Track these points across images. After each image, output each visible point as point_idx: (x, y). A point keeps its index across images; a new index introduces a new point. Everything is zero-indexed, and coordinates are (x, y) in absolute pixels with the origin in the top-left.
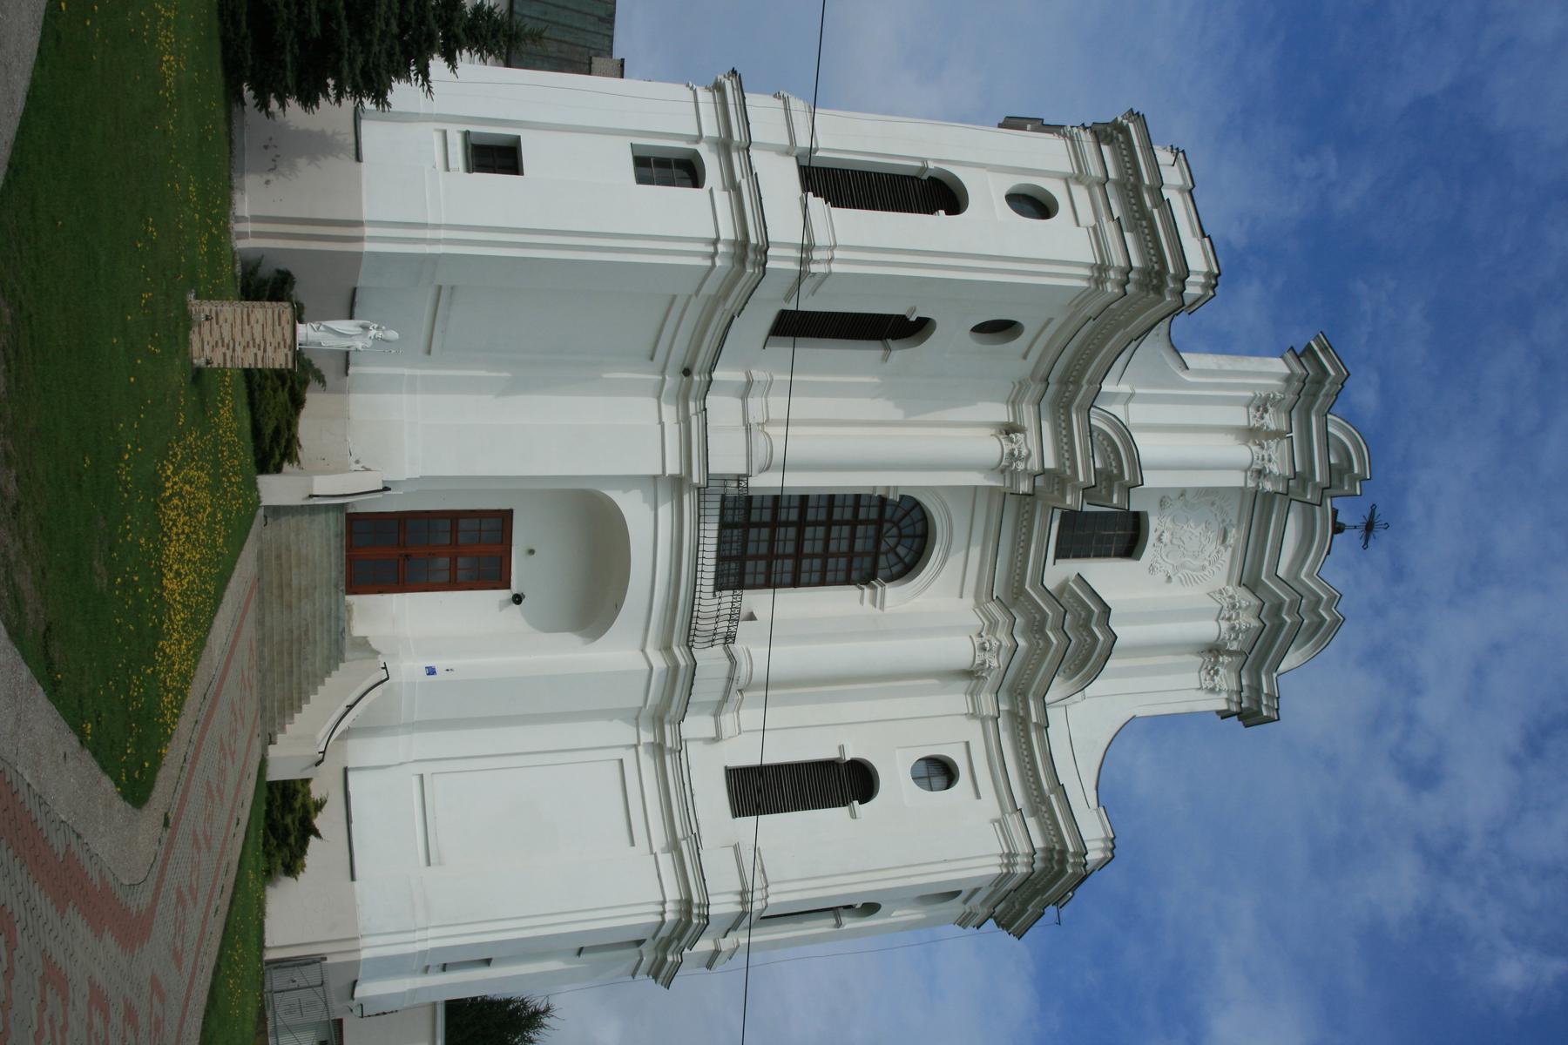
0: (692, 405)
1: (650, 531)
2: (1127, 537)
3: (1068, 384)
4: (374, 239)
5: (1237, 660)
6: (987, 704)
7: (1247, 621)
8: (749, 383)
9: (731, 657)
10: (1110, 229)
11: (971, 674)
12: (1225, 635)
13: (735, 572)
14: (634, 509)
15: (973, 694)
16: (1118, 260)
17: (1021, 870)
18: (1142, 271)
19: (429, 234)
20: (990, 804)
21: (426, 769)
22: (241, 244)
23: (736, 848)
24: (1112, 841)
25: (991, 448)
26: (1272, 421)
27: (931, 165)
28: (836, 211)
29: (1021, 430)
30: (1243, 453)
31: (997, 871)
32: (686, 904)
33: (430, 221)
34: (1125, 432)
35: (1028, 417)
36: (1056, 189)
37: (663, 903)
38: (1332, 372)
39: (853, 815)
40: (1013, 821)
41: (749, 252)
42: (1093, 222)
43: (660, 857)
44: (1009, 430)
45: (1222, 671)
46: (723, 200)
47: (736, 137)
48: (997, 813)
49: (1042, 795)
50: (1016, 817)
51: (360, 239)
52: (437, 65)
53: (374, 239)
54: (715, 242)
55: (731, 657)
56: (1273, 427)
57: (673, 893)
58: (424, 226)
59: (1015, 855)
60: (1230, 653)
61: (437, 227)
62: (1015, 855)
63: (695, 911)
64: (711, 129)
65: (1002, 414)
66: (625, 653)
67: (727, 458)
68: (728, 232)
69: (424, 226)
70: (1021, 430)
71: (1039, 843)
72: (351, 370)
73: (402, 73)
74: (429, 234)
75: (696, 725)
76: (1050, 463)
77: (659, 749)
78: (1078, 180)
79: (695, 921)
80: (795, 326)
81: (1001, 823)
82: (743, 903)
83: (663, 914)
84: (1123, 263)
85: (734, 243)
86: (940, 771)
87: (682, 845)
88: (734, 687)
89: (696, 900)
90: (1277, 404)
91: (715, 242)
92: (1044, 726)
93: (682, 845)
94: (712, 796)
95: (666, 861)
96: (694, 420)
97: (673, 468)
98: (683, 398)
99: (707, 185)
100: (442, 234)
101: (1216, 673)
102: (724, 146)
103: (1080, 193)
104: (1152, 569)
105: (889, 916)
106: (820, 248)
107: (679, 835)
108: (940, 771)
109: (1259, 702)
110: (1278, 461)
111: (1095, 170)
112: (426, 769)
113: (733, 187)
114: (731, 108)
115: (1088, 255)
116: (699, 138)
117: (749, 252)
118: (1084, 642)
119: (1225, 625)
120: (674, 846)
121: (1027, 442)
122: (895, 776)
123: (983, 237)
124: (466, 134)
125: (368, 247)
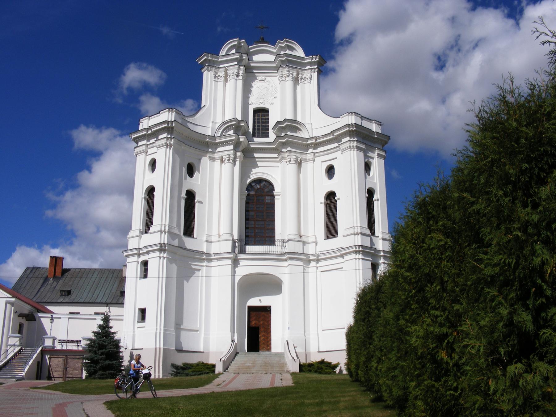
0: (212, 257)
1: (246, 268)
2: (262, 113)
3: (206, 145)
4: (160, 345)
5: (301, 72)
6: (309, 157)
7: (285, 71)
8: (207, 241)
9: (288, 241)
10: (158, 143)
11: (299, 163)
12: (290, 78)
13: (270, 239)
14: (243, 270)
15: (306, 161)
16: (164, 141)
17: (355, 144)
18: (168, 134)
19: (158, 331)
20: (338, 154)
21: (320, 329)
22: (161, 377)
23: (69, 318)
24: (349, 113)
25: (227, 166)
26: (221, 73)
27: (143, 196)
28: (154, 224)
29: (222, 157)
30: (231, 82)
31: (355, 152)
32: (356, 252)
33: (132, 333)
34: (224, 123)
35: (217, 155)
36: (149, 159)
37: (356, 259)
38: (206, 57)
39: (339, 199)
40: (342, 147)
41: (162, 248)
42: (156, 148)
43: (345, 260)
44: (222, 161)
45: (305, 76)
46: (151, 255)
47: (136, 252)
48: (340, 152)
49: (335, 138)
50: (341, 146)
51: (160, 348)
52: (112, 330)
53: (160, 345)
54: (160, 257)
55: (288, 241)
56: (224, 73)
57: (353, 256)
58: (156, 333)
59: (350, 146)
60: (298, 74)
61: (156, 329)
62: (350, 146)
63: (357, 249)
64: (135, 258)
65: (218, 163)
66: (284, 271)
67: (227, 247)
68: (157, 254)
69: (156, 333)
70: (222, 157)
71: (348, 139)
72: (202, 351)
73: (113, 337)
74: (158, 331)
75: (310, 250)
76: (231, 147)
77: (318, 261)
78: (147, 153)
79: (361, 249)
80: (189, 231)
81: (343, 151)
82: (358, 234)
83: (359, 259)
84: (165, 139)
85: (161, 253)
86: (330, 171)
87: (342, 253)
88: (300, 238)
89: (354, 249)
90: (216, 73)
91: (160, 257)
92: (316, 138)
93: (342, 253)
94: (334, 243)
95: (346, 258)
96: (217, 257)
97: (229, 262)
98: (210, 260)
99: (147, 259)
100: (158, 328)
101: (305, 78)
102: (139, 255)
103: (150, 151)
104: (272, 104)
105: (376, 183)
106: (161, 229)
107: (339, 254)
108: (330, 171)
109: (315, 62)
110: (233, 70)
111: (143, 148)
112: (320, 329)
113: (148, 253)
114: (130, 253)
115: (164, 149)
116: (138, 262)
117: (162, 248)
118: (290, 126)
119: (288, 79)
120: (342, 256)
121: (225, 156)
122: (330, 185)
123: (161, 180)
124: (138, 322)
125: (162, 346)
